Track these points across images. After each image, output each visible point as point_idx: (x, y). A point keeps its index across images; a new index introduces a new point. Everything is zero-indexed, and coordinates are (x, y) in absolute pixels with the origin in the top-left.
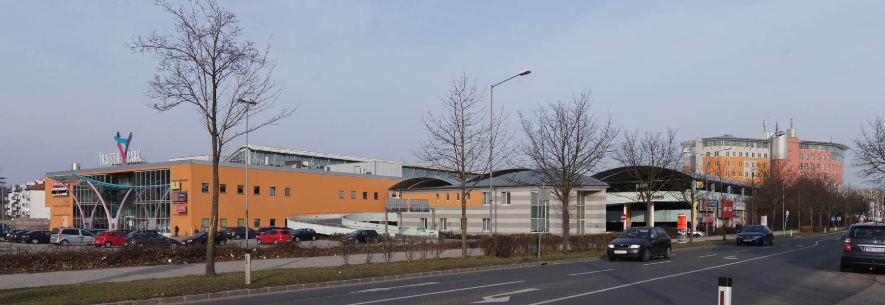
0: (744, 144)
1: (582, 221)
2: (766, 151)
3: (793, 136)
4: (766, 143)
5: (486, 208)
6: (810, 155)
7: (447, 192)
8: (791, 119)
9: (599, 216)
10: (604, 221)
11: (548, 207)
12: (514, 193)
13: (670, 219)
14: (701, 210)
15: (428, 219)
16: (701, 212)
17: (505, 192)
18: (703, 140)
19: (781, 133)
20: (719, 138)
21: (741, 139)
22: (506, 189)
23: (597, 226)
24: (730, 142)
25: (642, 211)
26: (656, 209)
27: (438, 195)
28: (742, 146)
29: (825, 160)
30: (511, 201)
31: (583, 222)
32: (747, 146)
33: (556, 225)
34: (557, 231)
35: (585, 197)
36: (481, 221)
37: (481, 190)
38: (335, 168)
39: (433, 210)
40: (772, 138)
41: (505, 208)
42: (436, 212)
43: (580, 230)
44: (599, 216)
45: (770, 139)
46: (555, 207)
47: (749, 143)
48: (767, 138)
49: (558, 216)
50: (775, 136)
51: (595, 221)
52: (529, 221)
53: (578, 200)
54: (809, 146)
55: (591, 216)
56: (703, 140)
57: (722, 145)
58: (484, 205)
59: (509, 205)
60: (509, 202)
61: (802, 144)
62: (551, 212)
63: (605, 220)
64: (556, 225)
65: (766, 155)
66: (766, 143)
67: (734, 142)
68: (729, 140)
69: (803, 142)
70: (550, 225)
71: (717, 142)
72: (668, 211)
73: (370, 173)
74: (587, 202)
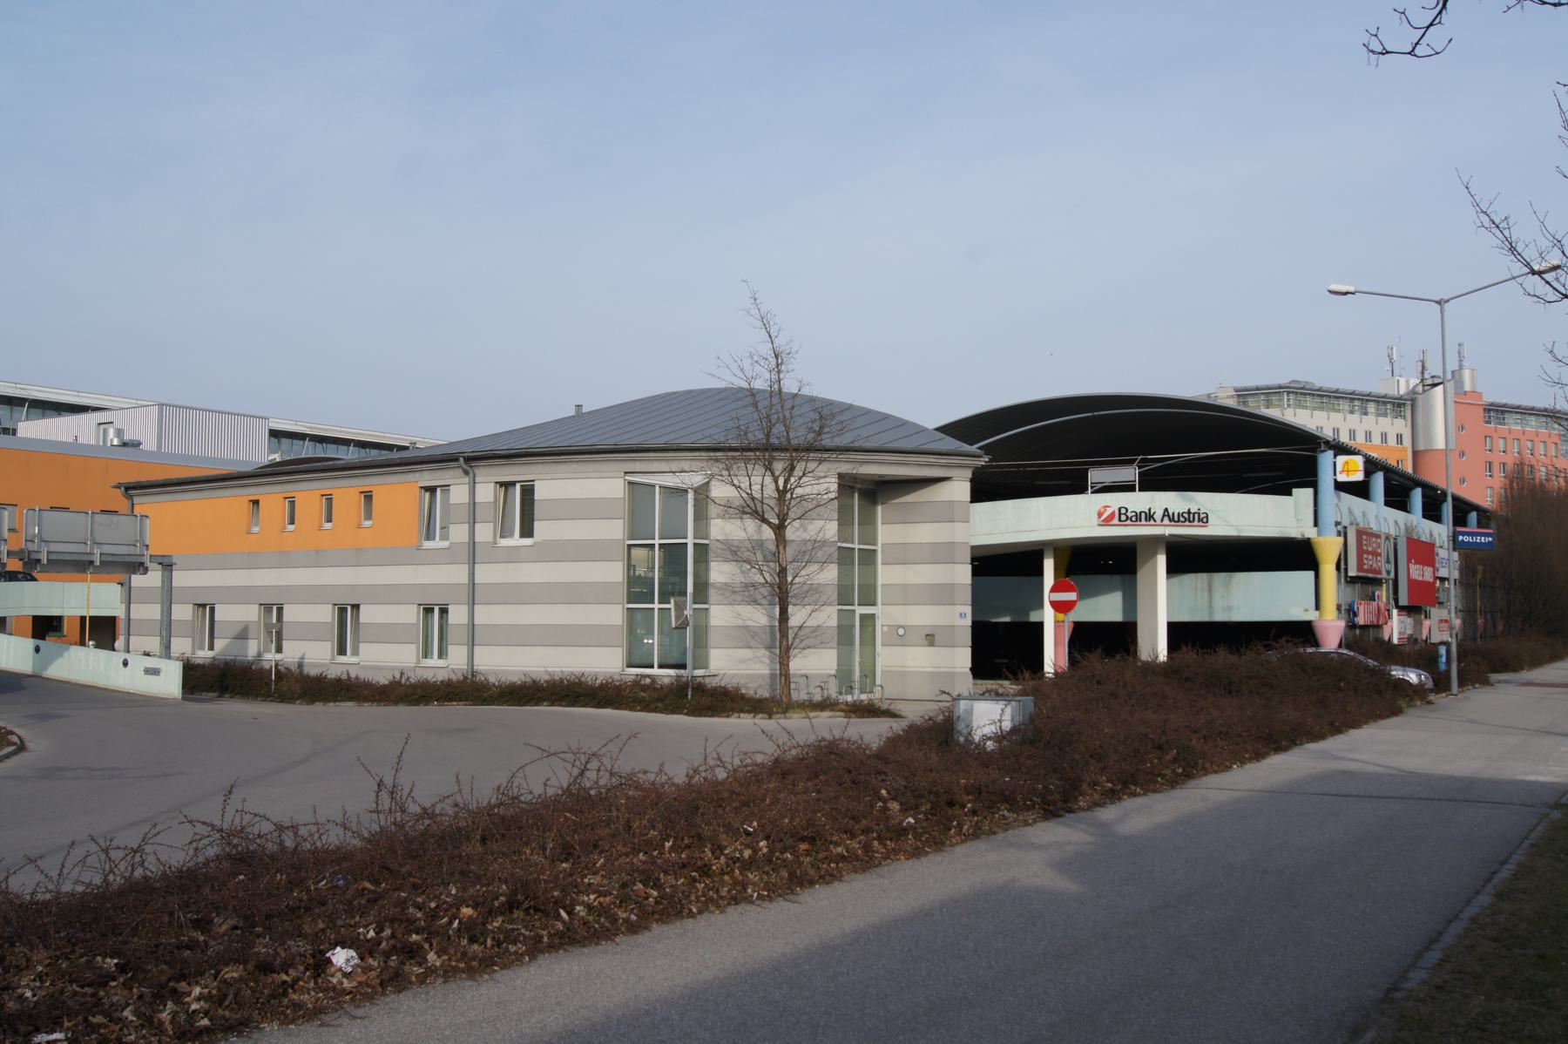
0: (1344, 405)
1: (863, 617)
2: (1401, 426)
3: (1467, 387)
4: (1399, 405)
5: (447, 557)
6: (1509, 441)
7: (290, 489)
8: (1460, 345)
9: (940, 595)
10: (961, 617)
11: (702, 551)
12: (552, 485)
13: (1230, 608)
14: (1351, 574)
15: (285, 607)
16: (1352, 581)
17: (513, 484)
18: (1236, 391)
19: (1437, 381)
20: (1280, 387)
21: (1336, 392)
22: (515, 469)
23: (930, 639)
24: (1308, 398)
25: (1117, 578)
26: (1172, 570)
27: (256, 503)
28: (1339, 411)
29: (1545, 455)
30: (537, 525)
31: (868, 620)
32: (1352, 412)
33: (745, 637)
34: (743, 661)
35: (879, 508)
36: (410, 615)
37: (411, 477)
38: (32, 429)
39: (167, 566)
40: (1413, 392)
41: (513, 556)
42: (180, 579)
43: (857, 659)
44: (940, 595)
45: (1408, 394)
46: (733, 552)
47: (1356, 403)
48: (1402, 392)
49: (745, 593)
50: (1420, 388)
51: (924, 616)
52: (614, 615)
53: (844, 520)
54: (1506, 416)
55: (908, 594)
56: (1236, 391)
57: (1289, 406)
58: (428, 544)
59: (527, 541)
60: (527, 531)
61: (1489, 410)
62: (719, 572)
63: (968, 610)
64: (745, 637)
65: (1399, 438)
66: (1399, 405)
67: (1318, 400)
68: (1305, 394)
69: (1492, 404)
70: (713, 637)
71: (1274, 398)
72: (1219, 578)
73: (137, 444)
74: (890, 530)
